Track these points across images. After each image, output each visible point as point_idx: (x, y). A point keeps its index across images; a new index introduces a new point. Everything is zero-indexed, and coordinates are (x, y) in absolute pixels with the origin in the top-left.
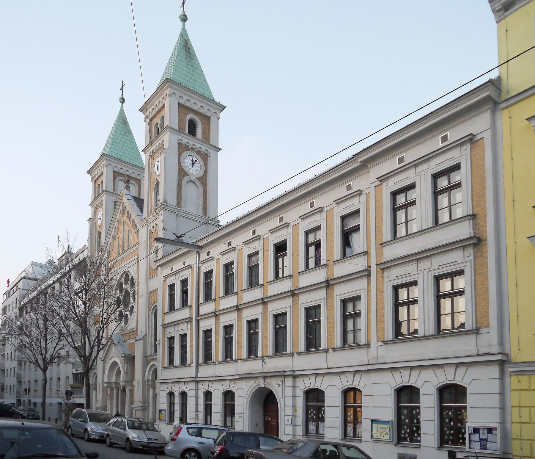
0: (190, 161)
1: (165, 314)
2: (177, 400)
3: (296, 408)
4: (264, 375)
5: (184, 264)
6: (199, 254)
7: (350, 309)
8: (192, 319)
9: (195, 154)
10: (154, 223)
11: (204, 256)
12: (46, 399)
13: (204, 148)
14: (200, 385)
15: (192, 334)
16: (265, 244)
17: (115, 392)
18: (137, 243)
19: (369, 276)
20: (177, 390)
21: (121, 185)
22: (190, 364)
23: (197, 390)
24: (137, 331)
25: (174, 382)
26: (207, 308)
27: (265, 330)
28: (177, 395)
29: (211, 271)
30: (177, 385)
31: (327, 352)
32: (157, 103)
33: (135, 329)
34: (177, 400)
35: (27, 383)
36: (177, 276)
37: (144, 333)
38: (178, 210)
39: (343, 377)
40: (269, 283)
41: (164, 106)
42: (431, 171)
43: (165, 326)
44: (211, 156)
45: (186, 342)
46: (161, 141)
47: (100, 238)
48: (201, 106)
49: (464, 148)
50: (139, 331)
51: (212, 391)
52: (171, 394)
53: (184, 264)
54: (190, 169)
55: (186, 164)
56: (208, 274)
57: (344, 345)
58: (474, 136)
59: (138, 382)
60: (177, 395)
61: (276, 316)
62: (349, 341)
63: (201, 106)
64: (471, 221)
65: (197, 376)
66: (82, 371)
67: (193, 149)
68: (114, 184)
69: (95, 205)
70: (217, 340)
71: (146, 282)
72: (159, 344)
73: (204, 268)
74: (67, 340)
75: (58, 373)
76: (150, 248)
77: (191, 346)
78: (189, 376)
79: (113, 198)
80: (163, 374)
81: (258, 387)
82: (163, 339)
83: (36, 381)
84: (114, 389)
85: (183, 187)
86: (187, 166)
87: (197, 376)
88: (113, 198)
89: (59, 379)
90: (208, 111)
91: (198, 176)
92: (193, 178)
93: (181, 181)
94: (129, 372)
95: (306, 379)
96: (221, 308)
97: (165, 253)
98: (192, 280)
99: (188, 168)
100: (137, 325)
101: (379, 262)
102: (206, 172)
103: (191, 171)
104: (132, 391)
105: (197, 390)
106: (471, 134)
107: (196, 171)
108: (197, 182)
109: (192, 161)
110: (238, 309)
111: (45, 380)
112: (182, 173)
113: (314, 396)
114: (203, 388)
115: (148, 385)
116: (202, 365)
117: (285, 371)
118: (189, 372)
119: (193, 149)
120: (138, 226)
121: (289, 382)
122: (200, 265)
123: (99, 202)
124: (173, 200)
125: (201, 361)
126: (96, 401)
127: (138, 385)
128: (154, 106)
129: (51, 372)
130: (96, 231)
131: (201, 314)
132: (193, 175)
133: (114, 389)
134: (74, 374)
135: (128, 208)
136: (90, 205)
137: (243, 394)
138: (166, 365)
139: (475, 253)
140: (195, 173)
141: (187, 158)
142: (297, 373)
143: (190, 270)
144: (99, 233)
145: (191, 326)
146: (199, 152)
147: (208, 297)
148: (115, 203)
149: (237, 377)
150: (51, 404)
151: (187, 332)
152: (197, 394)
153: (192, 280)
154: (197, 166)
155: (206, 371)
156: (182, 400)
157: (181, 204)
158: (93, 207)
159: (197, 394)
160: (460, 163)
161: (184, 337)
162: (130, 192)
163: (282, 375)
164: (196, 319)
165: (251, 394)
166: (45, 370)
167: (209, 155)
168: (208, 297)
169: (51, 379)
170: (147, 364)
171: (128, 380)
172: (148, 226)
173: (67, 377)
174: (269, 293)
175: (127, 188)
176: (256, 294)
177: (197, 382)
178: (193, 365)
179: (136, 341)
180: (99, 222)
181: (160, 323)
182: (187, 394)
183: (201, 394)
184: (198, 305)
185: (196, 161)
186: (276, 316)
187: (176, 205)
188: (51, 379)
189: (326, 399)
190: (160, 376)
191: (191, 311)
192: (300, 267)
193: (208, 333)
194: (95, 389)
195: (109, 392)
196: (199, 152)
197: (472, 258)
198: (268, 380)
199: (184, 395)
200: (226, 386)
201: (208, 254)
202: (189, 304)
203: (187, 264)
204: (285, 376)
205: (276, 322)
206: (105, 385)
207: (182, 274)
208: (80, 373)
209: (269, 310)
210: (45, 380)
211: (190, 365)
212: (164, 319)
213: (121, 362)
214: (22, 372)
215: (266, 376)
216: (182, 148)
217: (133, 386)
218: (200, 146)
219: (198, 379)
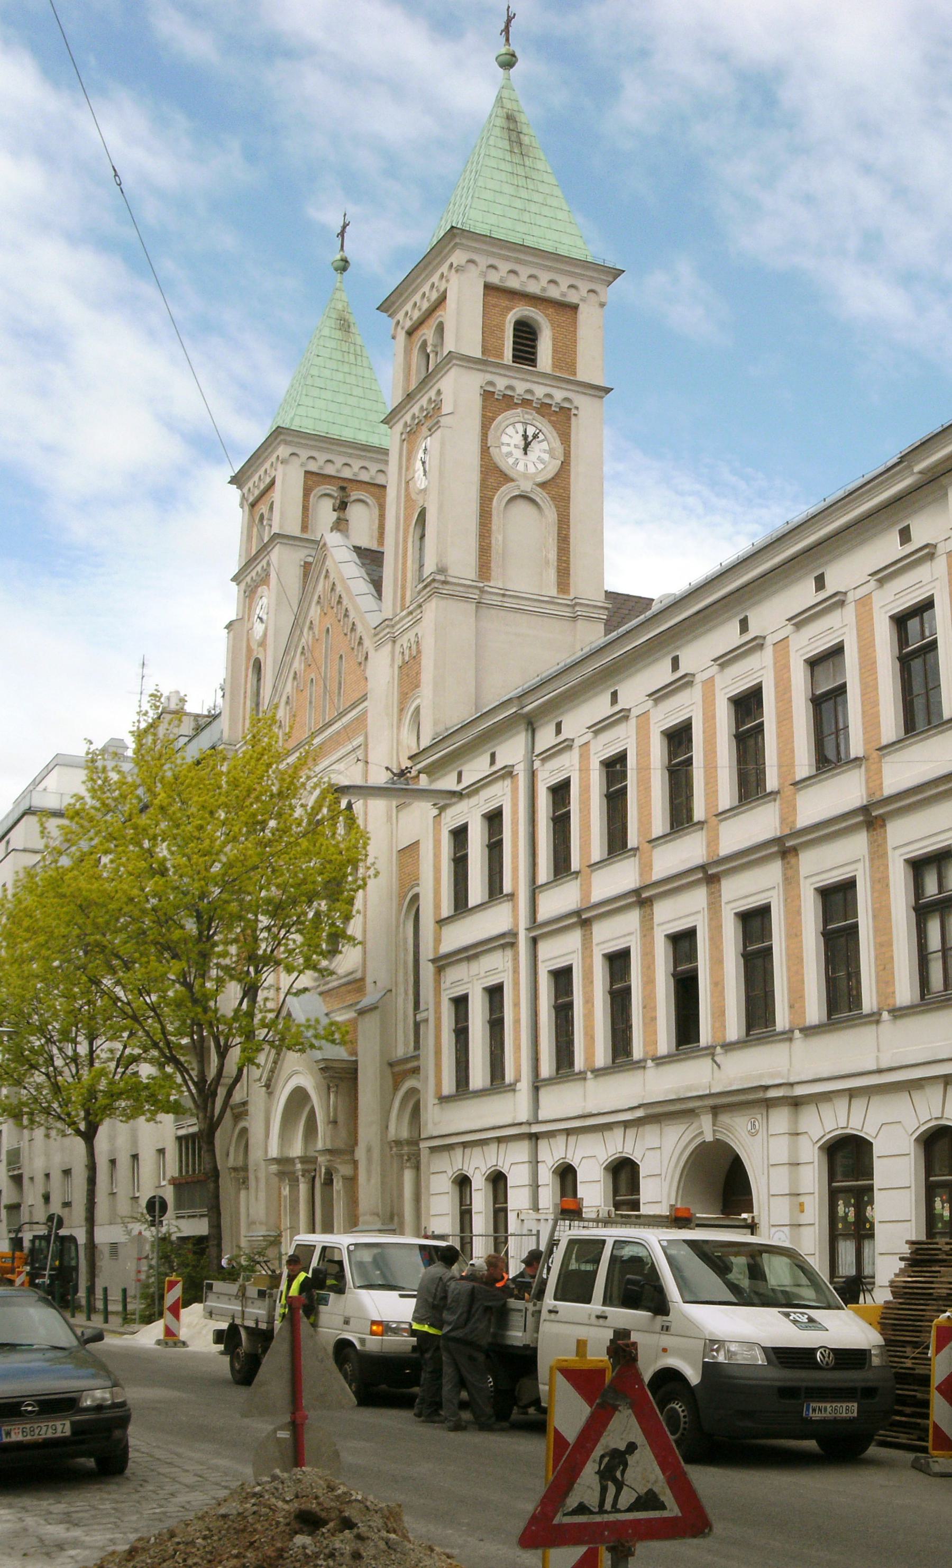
1: (441, 922)
2: (480, 1200)
3: (802, 1199)
4: (711, 1102)
5: (493, 762)
8: (515, 935)
9: (530, 416)
10: (411, 635)
11: (546, 738)
12: (96, 1229)
13: (559, 395)
15: (516, 983)
16: (782, 670)
17: (303, 1188)
18: (364, 698)
19: (513, 945)
20: (478, 1166)
21: (325, 512)
23: (535, 1162)
24: (362, 979)
26: (559, 901)
27: (794, 933)
28: (479, 1183)
29: (621, 758)
30: (477, 1151)
31: (878, 1022)
33: (358, 975)
34: (480, 1200)
35: (40, 1179)
36: (474, 800)
37: (383, 983)
38: (482, 590)
40: (798, 785)
43: (442, 963)
44: (581, 413)
45: (502, 1012)
47: (259, 680)
48: (531, 276)
50: (369, 980)
51: (575, 1164)
52: (463, 1182)
53: (493, 762)
54: (516, 462)
55: (505, 449)
56: (560, 791)
57: (923, 996)
59: (369, 1150)
60: (479, 1183)
63: (531, 276)
66: (194, 1129)
67: (526, 403)
68: (305, 509)
69: (251, 576)
70: (589, 1000)
71: (389, 818)
72: (426, 1020)
73: (547, 777)
74: (92, 1052)
75: (134, 1141)
76: (401, 710)
77: (517, 1021)
78: (509, 1121)
80: (442, 1121)
81: (698, 1141)
82: (438, 1004)
83: (67, 1172)
84: (301, 1179)
85: (495, 519)
86: (510, 454)
88: (299, 555)
89: (135, 1157)
90: (552, 286)
91: (540, 479)
92: (526, 486)
93: (491, 500)
94: (341, 1119)
95: (826, 1109)
96: (655, 877)
97: (441, 728)
98: (515, 812)
99: (511, 461)
100: (364, 960)
102: (565, 465)
103: (521, 467)
104: (351, 1181)
105: (535, 1162)
107: (534, 465)
108: (540, 496)
109: (525, 436)
110: (641, 899)
111: (92, 1167)
112: (492, 475)
113: (848, 1159)
114: (552, 1154)
115: (392, 1156)
116: (550, 1081)
117: (766, 1088)
118: (512, 1109)
119: (526, 403)
120: (367, 643)
121: (780, 1119)
122: (537, 764)
123: (259, 568)
124: (463, 566)
125: (547, 1068)
126: (251, 1224)
127: (369, 1160)
129: (112, 1138)
130: (248, 659)
131: (542, 916)
132: (526, 476)
133: (301, 1179)
134: (179, 1139)
136: (234, 579)
137: (662, 1164)
139: (783, 865)
140: (532, 470)
142: (799, 1091)
143: (508, 782)
144: (258, 667)
145: (516, 959)
146: (544, 409)
147: (561, 866)
148: (307, 566)
149: (640, 1113)
150: (114, 1247)
151: (506, 979)
152: (535, 1175)
153: (515, 812)
154: (538, 449)
155: (561, 1103)
156: (495, 1201)
157: (489, 568)
158: (243, 585)
159: (535, 1175)
161: (495, 993)
162: (347, 537)
163: (756, 1100)
165: (682, 1164)
166: (89, 1136)
167: (574, 411)
168: (561, 866)
169: (113, 1162)
170: (396, 1087)
171: (340, 1144)
172: (394, 642)
173: (161, 1151)
174: (886, 783)
175: (340, 525)
176: (844, 793)
178: (524, 1086)
179: (361, 1013)
180: (259, 629)
181: (427, 952)
182: (506, 1178)
183: (546, 1176)
184: (535, 890)
185: (535, 436)
187: (473, 576)
188: (113, 1162)
189: (878, 1165)
190: (430, 1126)
191: (515, 909)
192: (883, 728)
193: (562, 978)
194: (244, 1182)
195: (286, 1191)
196: (544, 409)
198: (725, 1119)
199: (498, 1180)
201: (558, 730)
203: (499, 764)
204: (769, 1104)
206: (274, 1168)
207: (485, 794)
208: (193, 1136)
209: (724, 899)
210: (92, 1167)
211: (512, 1088)
212: (438, 940)
213: (317, 1088)
214: (24, 1144)
215: (723, 1104)
217: (355, 1163)
218: (548, 390)
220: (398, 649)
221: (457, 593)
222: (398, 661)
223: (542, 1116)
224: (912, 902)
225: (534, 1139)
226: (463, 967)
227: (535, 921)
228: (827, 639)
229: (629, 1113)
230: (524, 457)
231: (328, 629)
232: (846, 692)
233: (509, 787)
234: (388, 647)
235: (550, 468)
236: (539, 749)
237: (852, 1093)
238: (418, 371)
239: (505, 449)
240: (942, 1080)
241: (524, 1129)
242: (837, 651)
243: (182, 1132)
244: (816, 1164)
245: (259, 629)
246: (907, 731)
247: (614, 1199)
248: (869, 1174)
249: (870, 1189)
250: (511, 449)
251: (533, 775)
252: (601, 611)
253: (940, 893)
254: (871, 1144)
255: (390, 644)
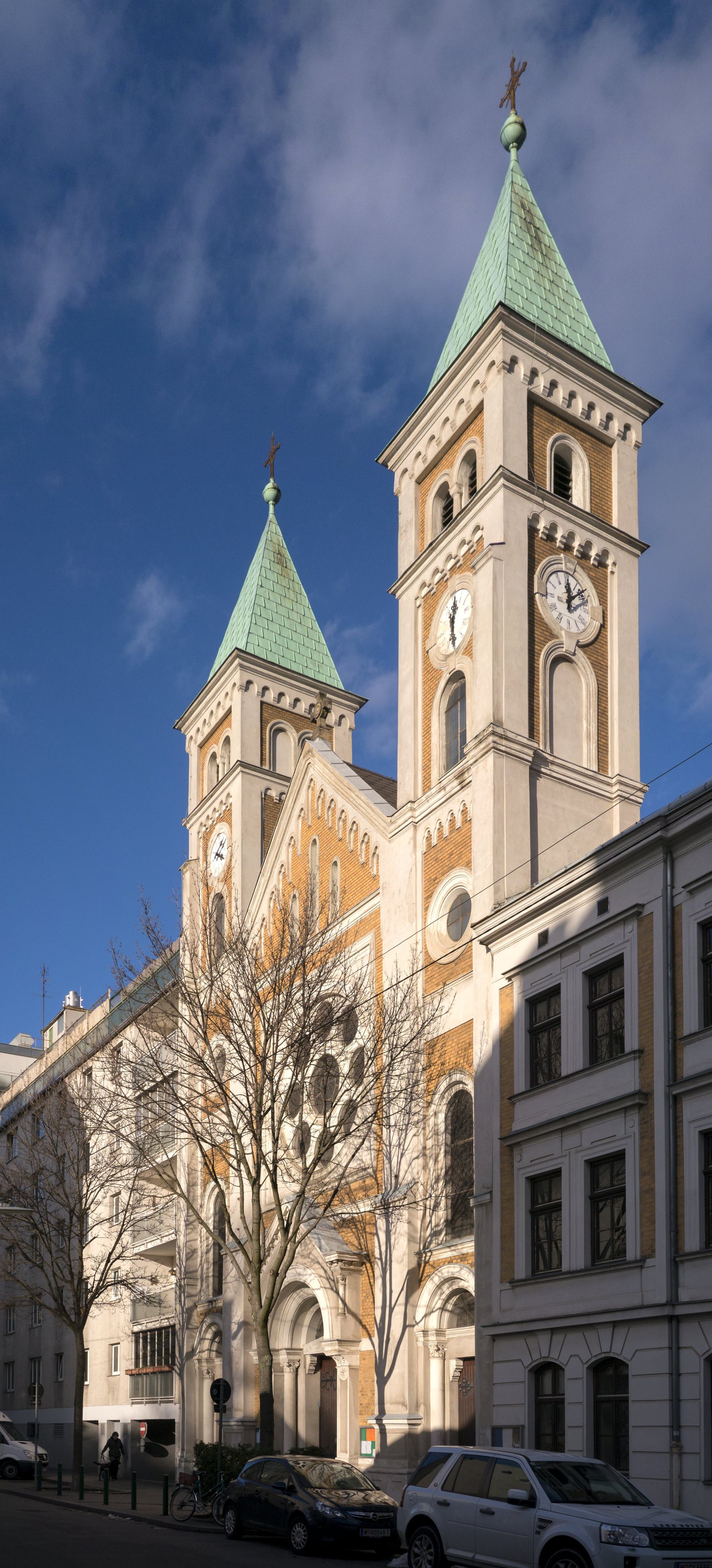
0: (561, 591)
6: (670, 860)
7: (605, 1181)
14: (660, 1335)
22: (643, 1259)
23: (675, 1349)
25: (559, 1328)
32: (213, 706)
39: (590, 1335)
41: (229, 712)
42: (582, 966)
46: (223, 797)
49: (629, 927)
54: (560, 618)
58: (643, 906)
61: (534, 1181)
62: (606, 1254)
64: (637, 1061)
65: (674, 1300)
76: (428, 897)
77: (647, 1192)
78: (637, 1302)
79: (260, 784)
86: (553, 607)
87: (674, 1300)
89: (59, 1356)
99: (555, 614)
101: (505, 1134)
103: (564, 624)
105: (675, 1349)
106: (637, 905)
108: (581, 658)
109: (568, 590)
128: (199, 724)
135: (330, 793)
138: (521, 1269)
141: (553, 578)
160: (622, 954)
164: (667, 1096)
177: (674, 1320)
184: (676, 1042)
186: (534, 1181)
197: (636, 1129)
200: (603, 1344)
202: (631, 1042)
205: (593, 1180)
216: (538, 545)
219: (680, 1311)
220: (421, 834)
221: (513, 752)
222: (422, 846)
223: (684, 1296)
224: (529, 1207)
225: (674, 1323)
226: (555, 1140)
227: (675, 1080)
228: (600, 957)
229: (657, 1309)
230: (569, 614)
231: (315, 841)
232: (623, 997)
233: (635, 932)
234: (410, 832)
235: (590, 630)
236: (680, 882)
237: (615, 1324)
238: (210, 780)
239: (550, 600)
240: (549, 1332)
241: (666, 1311)
242: (617, 963)
243: (136, 1329)
244: (702, 1374)
245: (217, 867)
246: (532, 1085)
247: (536, 1399)
248: (626, 1390)
249: (626, 1400)
250: (555, 600)
251: (673, 914)
252: (639, 794)
253: (612, 1185)
254: (627, 1365)
255: (410, 832)
